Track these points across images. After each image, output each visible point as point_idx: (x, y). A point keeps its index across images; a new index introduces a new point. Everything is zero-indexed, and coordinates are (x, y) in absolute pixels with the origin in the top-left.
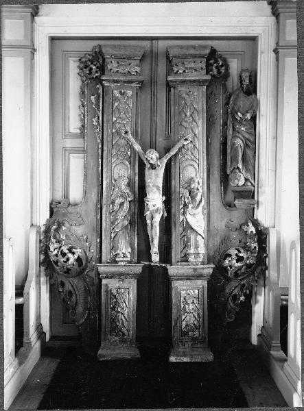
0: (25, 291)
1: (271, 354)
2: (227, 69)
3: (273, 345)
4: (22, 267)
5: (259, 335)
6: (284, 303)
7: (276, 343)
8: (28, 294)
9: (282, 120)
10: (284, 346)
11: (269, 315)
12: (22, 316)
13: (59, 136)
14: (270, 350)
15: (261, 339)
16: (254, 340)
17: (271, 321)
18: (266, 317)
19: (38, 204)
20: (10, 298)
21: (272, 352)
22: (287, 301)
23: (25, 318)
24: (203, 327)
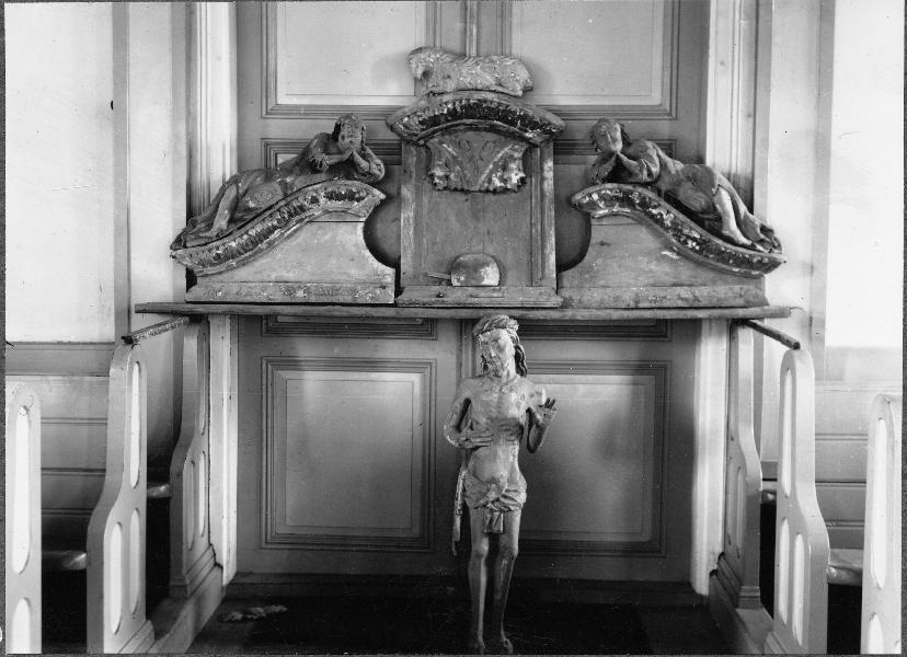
0: (173, 468)
1: (738, 615)
2: (534, 125)
3: (742, 594)
4: (169, 413)
5: (713, 573)
6: (770, 497)
7: (752, 590)
8: (180, 475)
9: (768, 75)
10: (768, 599)
11: (735, 527)
12: (167, 552)
13: (253, 114)
14: (737, 606)
15: (717, 582)
16: (702, 584)
17: (739, 541)
18: (730, 532)
19: (203, 16)
20: (134, 484)
21: (739, 611)
22: (774, 493)
23: (172, 522)
24: (509, 570)
